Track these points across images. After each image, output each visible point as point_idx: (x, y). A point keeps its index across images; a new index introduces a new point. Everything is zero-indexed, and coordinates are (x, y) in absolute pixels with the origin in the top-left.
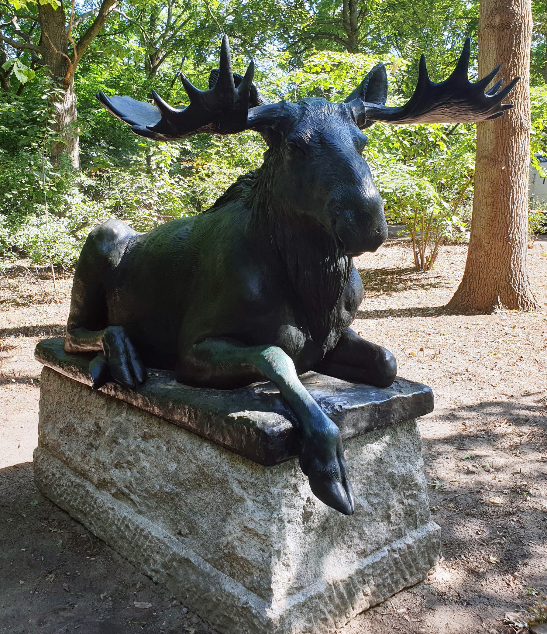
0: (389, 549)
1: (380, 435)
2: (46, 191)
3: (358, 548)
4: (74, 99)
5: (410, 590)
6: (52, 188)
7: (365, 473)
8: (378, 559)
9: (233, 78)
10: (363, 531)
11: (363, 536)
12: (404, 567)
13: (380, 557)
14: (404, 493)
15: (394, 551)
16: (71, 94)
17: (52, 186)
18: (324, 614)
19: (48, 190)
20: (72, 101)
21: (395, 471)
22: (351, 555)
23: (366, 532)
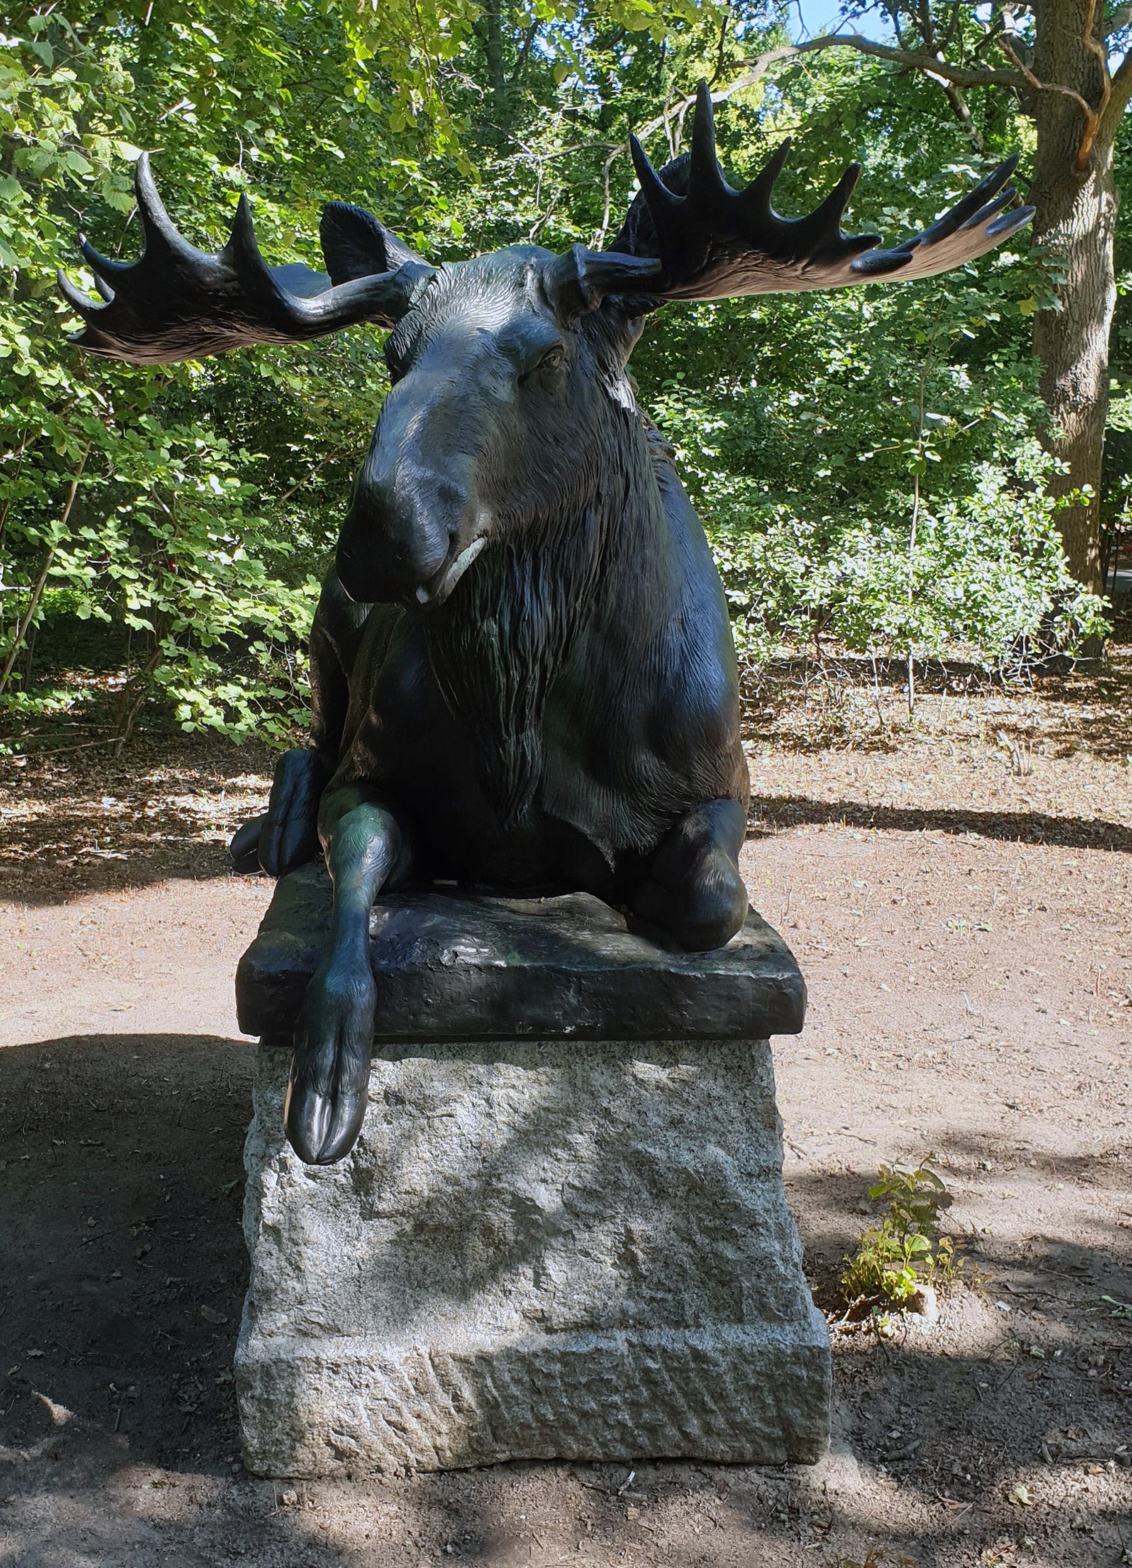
0: (634, 1340)
1: (618, 1055)
2: (914, 461)
3: (525, 1303)
4: (1104, 209)
5: (706, 1470)
6: (928, 454)
7: (559, 1132)
8: (584, 1349)
9: (620, 258)
10: (544, 1269)
11: (543, 1278)
12: (682, 1401)
13: (592, 1346)
14: (700, 1219)
15: (649, 1350)
16: (1097, 193)
17: (929, 449)
18: (400, 1413)
19: (918, 458)
20: (1099, 215)
21: (656, 1152)
22: (506, 1313)
23: (551, 1272)
